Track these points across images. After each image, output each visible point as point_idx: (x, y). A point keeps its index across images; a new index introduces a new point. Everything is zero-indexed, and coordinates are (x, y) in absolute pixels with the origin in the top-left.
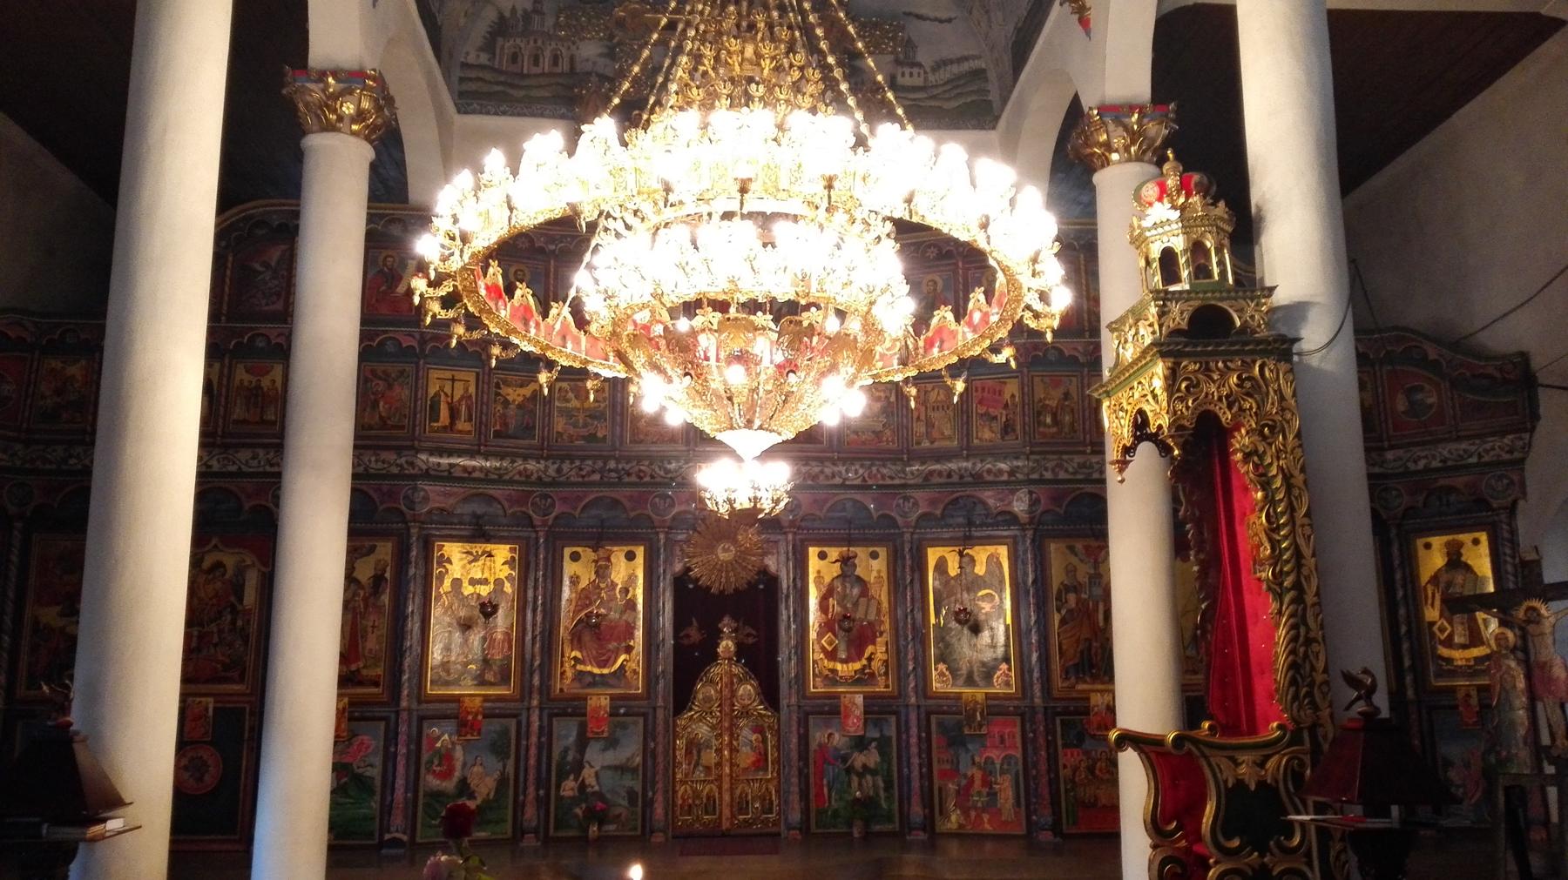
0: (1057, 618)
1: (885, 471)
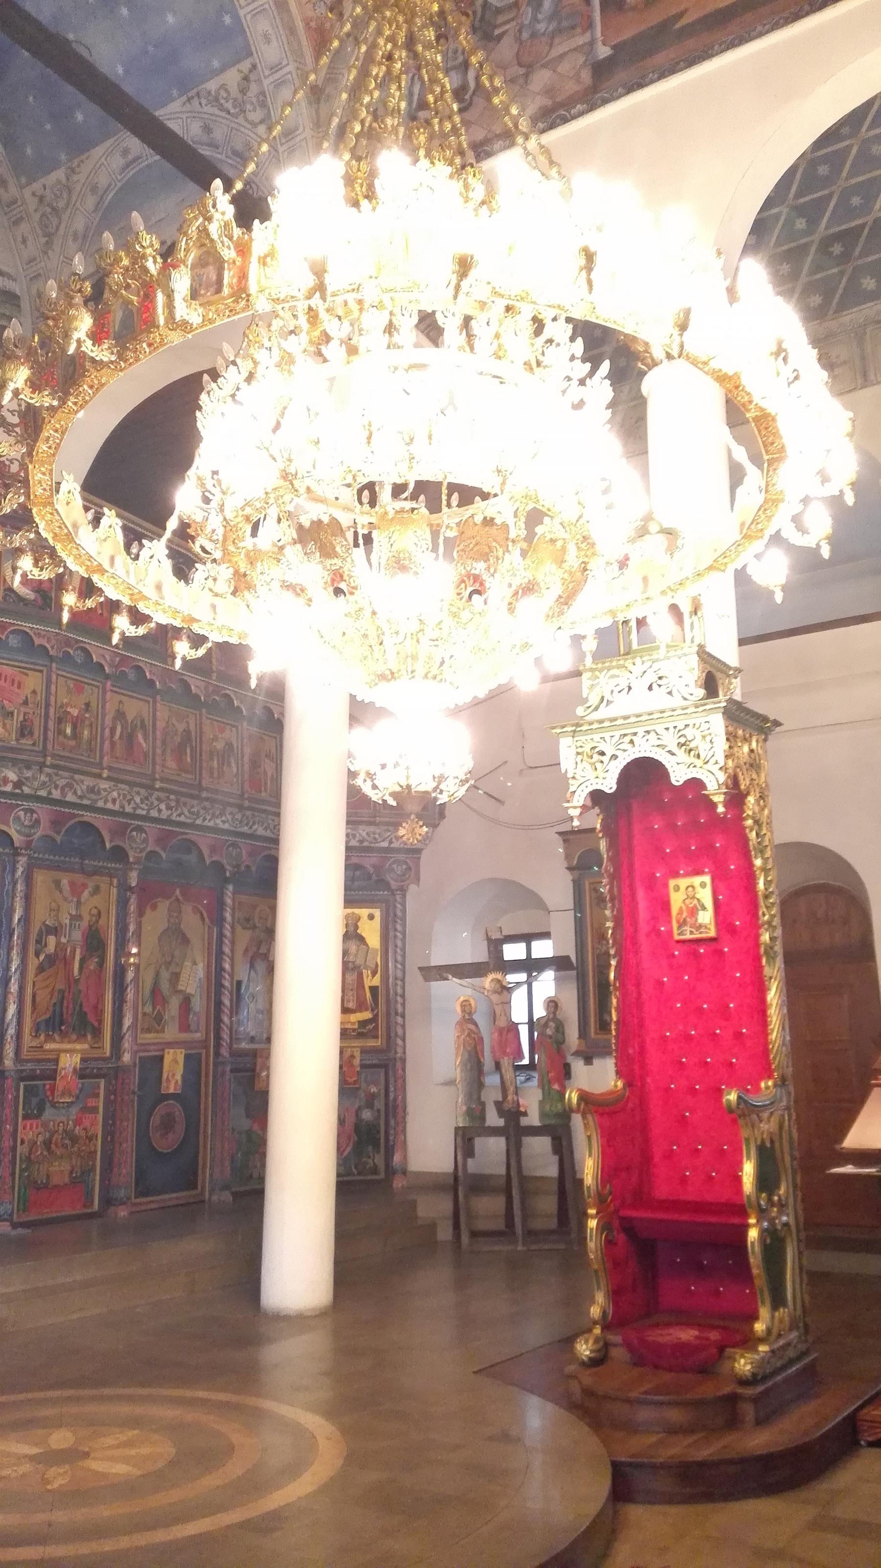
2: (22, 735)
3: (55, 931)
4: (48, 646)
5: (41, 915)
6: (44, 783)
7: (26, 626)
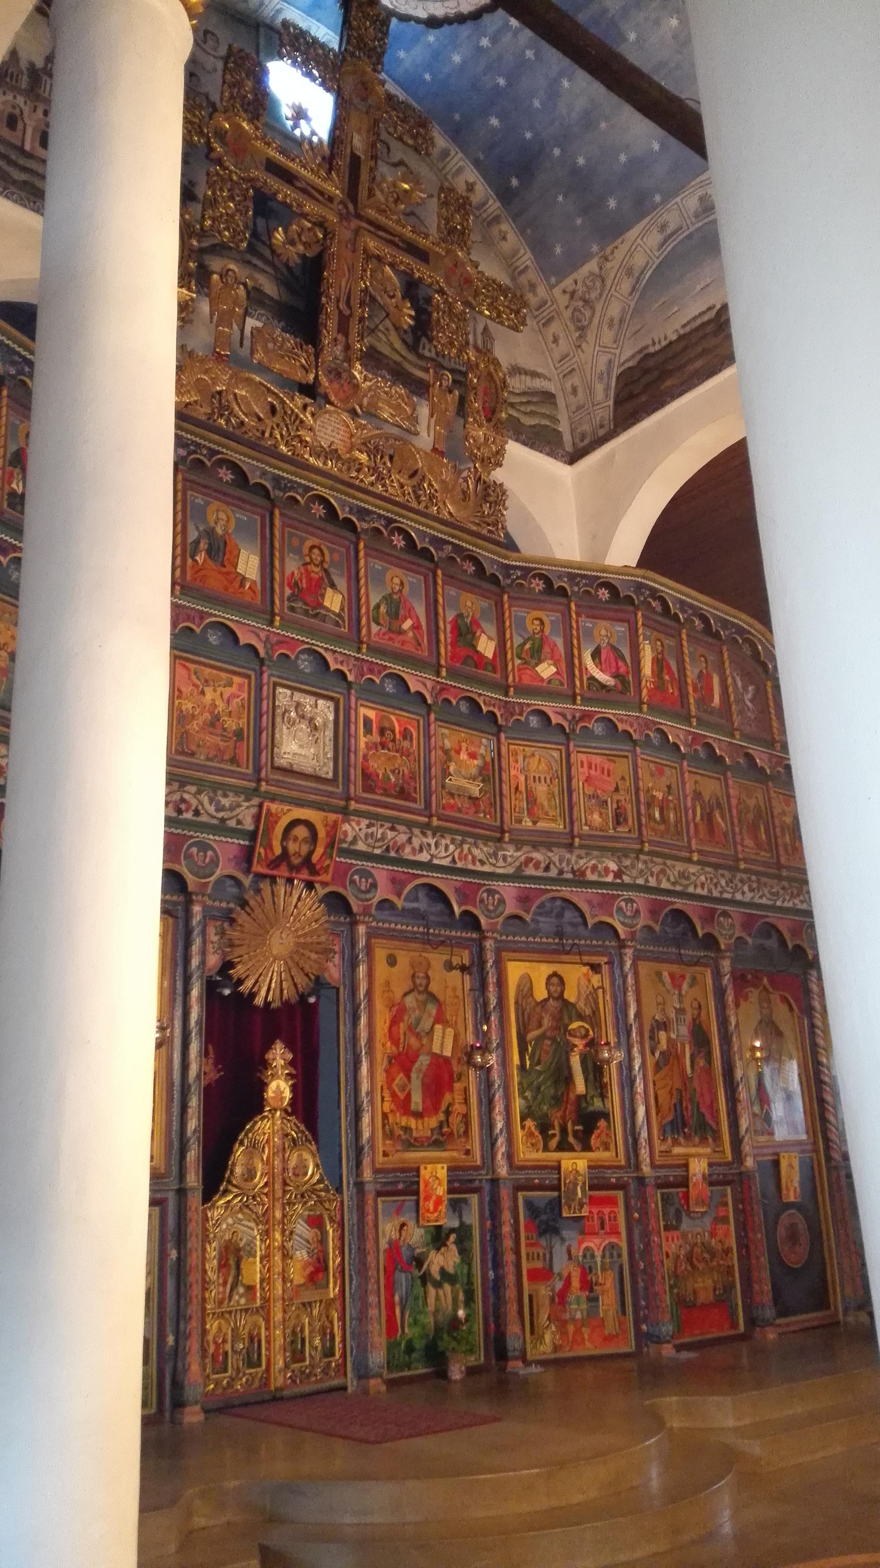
1: (476, 852)
2: (618, 823)
3: (664, 1025)
4: (631, 731)
5: (652, 1012)
6: (642, 871)
7: (610, 712)
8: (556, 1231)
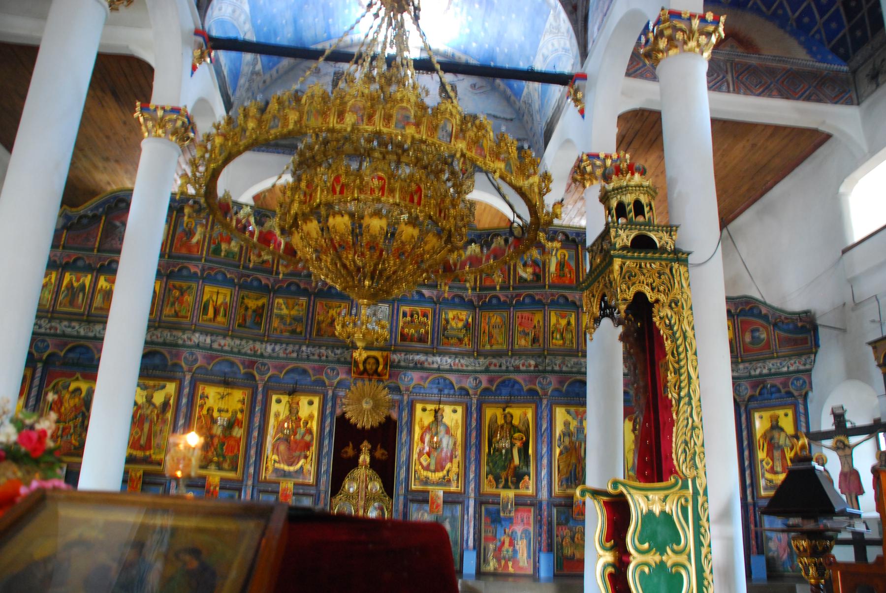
0: (558, 451)
1: (462, 361)
7: (531, 292)
8: (500, 522)
